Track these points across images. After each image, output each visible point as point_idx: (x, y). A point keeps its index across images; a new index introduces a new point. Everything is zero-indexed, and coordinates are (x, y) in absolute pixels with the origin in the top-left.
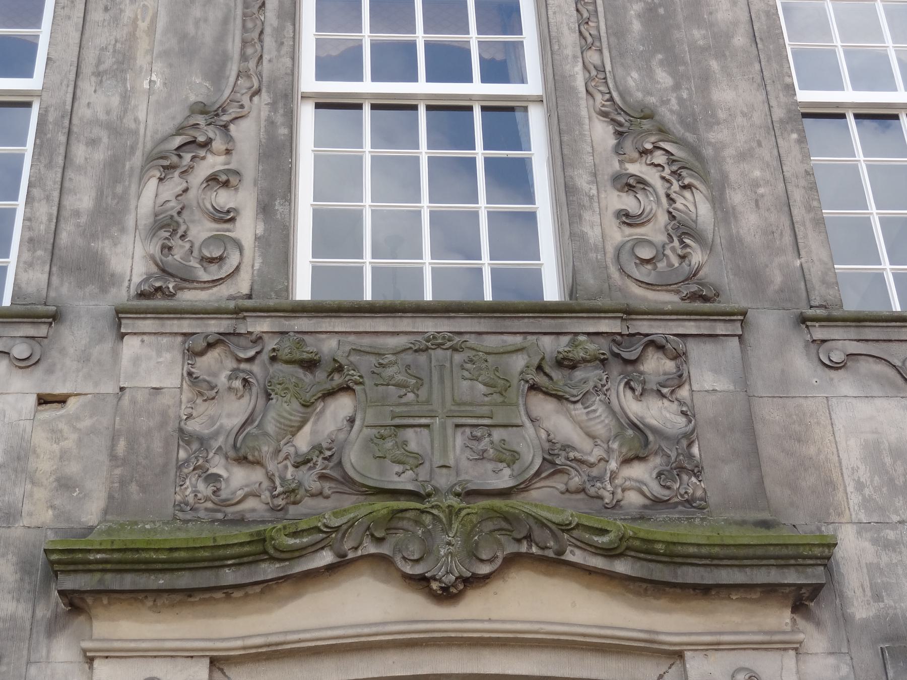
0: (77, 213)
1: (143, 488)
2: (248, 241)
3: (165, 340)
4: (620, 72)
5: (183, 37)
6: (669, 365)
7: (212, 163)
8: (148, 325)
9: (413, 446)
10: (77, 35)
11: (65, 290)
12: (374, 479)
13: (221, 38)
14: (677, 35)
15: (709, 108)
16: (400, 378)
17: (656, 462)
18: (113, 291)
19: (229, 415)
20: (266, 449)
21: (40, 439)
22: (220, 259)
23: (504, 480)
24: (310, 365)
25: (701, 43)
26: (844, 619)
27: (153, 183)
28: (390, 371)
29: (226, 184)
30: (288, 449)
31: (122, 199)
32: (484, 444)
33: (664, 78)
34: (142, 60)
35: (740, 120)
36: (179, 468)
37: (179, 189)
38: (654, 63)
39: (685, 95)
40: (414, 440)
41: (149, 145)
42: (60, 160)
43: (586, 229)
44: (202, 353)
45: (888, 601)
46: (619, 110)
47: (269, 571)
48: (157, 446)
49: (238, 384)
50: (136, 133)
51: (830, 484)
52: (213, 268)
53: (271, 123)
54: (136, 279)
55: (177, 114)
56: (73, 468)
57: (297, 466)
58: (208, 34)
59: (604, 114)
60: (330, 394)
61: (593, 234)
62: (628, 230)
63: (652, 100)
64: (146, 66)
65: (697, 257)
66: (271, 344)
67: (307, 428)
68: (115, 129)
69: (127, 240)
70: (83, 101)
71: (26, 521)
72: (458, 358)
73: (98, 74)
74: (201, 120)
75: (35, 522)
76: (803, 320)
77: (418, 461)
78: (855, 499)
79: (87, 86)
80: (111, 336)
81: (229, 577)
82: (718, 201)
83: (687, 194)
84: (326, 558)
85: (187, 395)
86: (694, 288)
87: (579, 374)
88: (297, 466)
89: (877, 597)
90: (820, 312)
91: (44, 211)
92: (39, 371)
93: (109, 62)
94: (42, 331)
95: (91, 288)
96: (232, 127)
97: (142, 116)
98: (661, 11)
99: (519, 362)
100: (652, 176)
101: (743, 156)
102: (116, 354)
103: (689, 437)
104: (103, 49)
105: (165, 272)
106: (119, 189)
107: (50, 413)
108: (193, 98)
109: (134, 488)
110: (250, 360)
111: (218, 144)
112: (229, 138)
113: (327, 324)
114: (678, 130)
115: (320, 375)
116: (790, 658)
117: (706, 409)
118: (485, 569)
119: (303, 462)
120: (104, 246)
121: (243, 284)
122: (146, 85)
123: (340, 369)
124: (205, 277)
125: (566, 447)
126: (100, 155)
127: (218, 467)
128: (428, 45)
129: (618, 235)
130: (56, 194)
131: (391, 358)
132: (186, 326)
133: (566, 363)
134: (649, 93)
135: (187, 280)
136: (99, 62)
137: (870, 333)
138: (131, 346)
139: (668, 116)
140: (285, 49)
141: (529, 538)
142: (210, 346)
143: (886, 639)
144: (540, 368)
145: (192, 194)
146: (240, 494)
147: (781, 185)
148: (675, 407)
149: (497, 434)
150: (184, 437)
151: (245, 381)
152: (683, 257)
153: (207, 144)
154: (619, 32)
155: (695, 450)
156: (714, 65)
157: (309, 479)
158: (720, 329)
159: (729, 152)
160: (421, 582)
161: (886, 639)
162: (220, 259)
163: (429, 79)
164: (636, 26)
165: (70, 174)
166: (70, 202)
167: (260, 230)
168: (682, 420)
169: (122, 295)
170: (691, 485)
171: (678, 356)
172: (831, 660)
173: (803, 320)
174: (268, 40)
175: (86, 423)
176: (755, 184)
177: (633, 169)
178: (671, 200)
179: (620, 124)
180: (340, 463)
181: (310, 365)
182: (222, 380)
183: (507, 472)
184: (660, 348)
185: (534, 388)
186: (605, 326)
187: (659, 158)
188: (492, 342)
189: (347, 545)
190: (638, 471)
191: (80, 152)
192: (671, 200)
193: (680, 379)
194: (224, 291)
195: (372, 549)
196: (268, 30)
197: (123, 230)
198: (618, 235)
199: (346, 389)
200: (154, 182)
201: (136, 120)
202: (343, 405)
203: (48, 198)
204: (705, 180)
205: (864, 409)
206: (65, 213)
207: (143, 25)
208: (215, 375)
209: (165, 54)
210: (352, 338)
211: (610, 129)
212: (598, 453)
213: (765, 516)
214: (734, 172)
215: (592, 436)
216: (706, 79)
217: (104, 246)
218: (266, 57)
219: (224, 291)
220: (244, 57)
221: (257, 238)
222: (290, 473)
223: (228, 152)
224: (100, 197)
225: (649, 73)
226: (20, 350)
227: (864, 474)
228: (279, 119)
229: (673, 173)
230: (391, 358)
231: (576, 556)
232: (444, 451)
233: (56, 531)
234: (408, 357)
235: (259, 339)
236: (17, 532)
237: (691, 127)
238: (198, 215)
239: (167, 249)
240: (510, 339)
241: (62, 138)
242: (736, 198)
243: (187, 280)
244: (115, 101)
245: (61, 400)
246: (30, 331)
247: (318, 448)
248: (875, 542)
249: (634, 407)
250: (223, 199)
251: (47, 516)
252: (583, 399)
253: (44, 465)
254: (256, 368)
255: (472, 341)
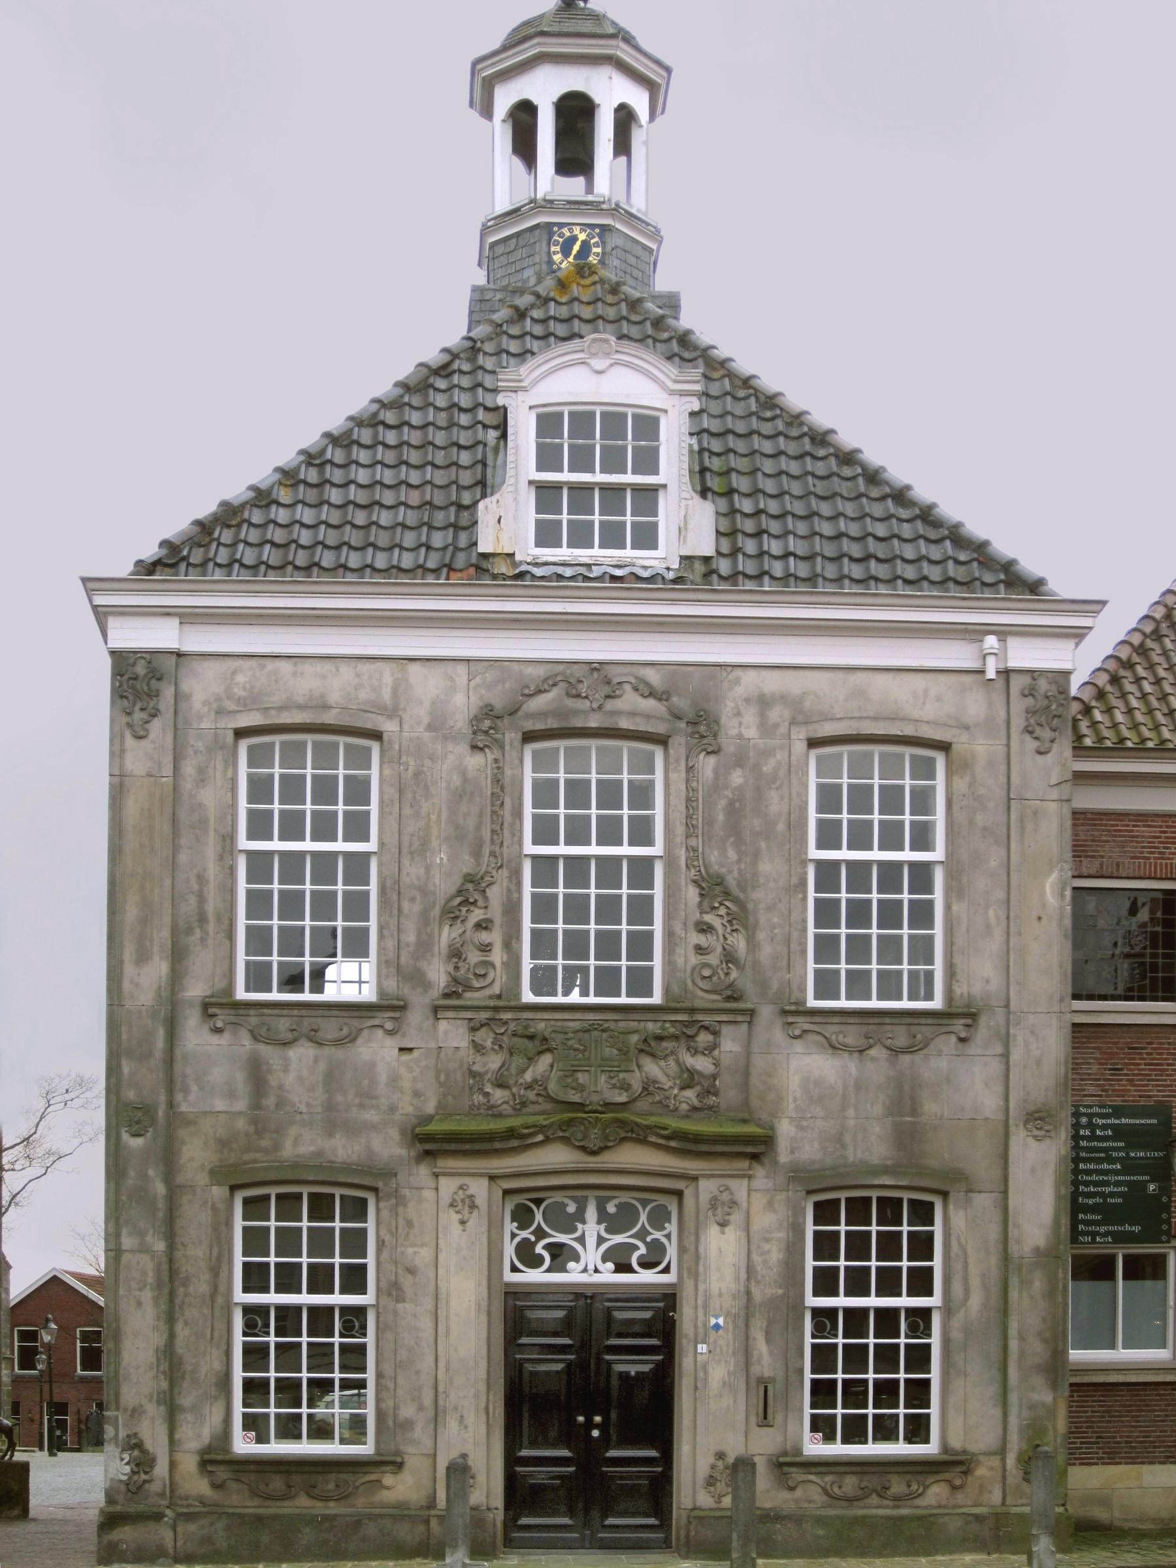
0: (408, 945)
1: (454, 1097)
2: (498, 964)
3: (459, 1022)
4: (707, 850)
5: (457, 826)
6: (710, 1038)
7: (477, 915)
8: (451, 1014)
9: (581, 1081)
10: (396, 826)
11: (406, 991)
12: (562, 1096)
13: (478, 827)
14: (744, 823)
15: (755, 875)
16: (576, 1046)
17: (698, 1088)
18: (431, 991)
19: (493, 1062)
20: (511, 1082)
21: (403, 1071)
22: (484, 976)
23: (622, 1098)
24: (531, 1037)
25: (758, 829)
26: (775, 1163)
27: (446, 929)
28: (570, 1043)
29: (486, 928)
30: (521, 1081)
31: (431, 936)
32: (614, 1081)
33: (732, 855)
34: (435, 843)
35: (772, 884)
36: (471, 1089)
37: (461, 931)
38: (728, 844)
39: (743, 866)
40: (582, 1078)
41: (443, 902)
42: (396, 912)
43: (676, 958)
44: (478, 1029)
45: (797, 1155)
46: (703, 879)
47: (515, 1143)
48: (459, 1076)
49: (496, 1047)
50: (434, 893)
51: (781, 1098)
52: (481, 980)
53: (509, 890)
54: (442, 985)
55: (456, 882)
56: (420, 1086)
57: (526, 1089)
58: (471, 824)
59: (695, 882)
60: (540, 1053)
61: (680, 961)
62: (700, 957)
63: (723, 870)
64: (437, 848)
65: (734, 974)
66: (512, 1026)
67: (530, 1069)
68: (423, 891)
69: (436, 961)
70: (404, 872)
71: (401, 1111)
72: (605, 1035)
73: (411, 853)
74: (470, 886)
75: (405, 1112)
76: (785, 1013)
77: (580, 1088)
78: (792, 1106)
79: (406, 862)
80: (431, 1021)
81: (497, 1145)
82: (751, 940)
83: (735, 934)
84: (540, 1138)
85: (471, 1051)
86: (729, 993)
87: (665, 1044)
88: (526, 1089)
89: (792, 1152)
90: (793, 1008)
91: (391, 944)
92: (398, 1036)
93: (416, 845)
94: (397, 1015)
95: (419, 990)
96: (487, 890)
97: (437, 882)
98: (737, 805)
99: (634, 1038)
100: (717, 923)
101: (770, 909)
102: (435, 1027)
103: (714, 1077)
104: (412, 835)
105: (456, 981)
106: (429, 930)
107: (406, 1057)
108: (465, 870)
109: (450, 1098)
110: (502, 1034)
111: (480, 903)
112: (486, 898)
113: (539, 1015)
114: (735, 891)
115: (537, 1042)
116: (745, 1182)
117: (726, 1061)
118: (611, 1144)
119: (529, 1087)
120: (423, 964)
121: (496, 989)
122: (438, 861)
123: (545, 1039)
124: (477, 985)
125: (655, 1082)
126: (417, 908)
127: (488, 1088)
128: (599, 782)
129: (694, 960)
130: (396, 934)
131: (571, 1035)
132: (469, 1015)
133: (660, 1038)
134: (722, 866)
135: (468, 987)
136: (411, 845)
137: (817, 1019)
138: (443, 1025)
139: (731, 882)
140: (516, 839)
141: (632, 1131)
142: (482, 1026)
143: (794, 1171)
144: (645, 1040)
145: (468, 933)
146: (499, 1102)
147: (787, 928)
148: (710, 1060)
149: (622, 1075)
150: (473, 1074)
151: (500, 1046)
152: (727, 974)
153: (475, 903)
154: (709, 822)
155: (717, 1083)
156: (763, 845)
157: (531, 1095)
158: (739, 1018)
159: (762, 906)
160: (583, 1149)
161: (794, 1171)
162: (484, 976)
163: (601, 472)
164: (721, 817)
165: (402, 920)
166: (403, 937)
167: (505, 959)
168: (713, 1067)
169: (435, 993)
170: (712, 1100)
171: (716, 1033)
172: (765, 1181)
173: (785, 1013)
174: (506, 833)
175: (423, 1063)
176: (773, 927)
177: (708, 918)
178: (725, 939)
179: (703, 888)
180: (546, 1089)
181: (531, 1037)
182: (489, 1043)
183: (625, 1094)
184: (706, 1028)
185: (642, 1051)
186: (680, 1017)
187: (722, 911)
188: (622, 1024)
189: (549, 1133)
190: (690, 1094)
191: (406, 905)
192: (725, 939)
193: (714, 1046)
194: (487, 992)
195: (561, 1134)
196: (506, 825)
197: (432, 955)
198: (694, 960)
199: (549, 1050)
200: (447, 927)
201: (434, 884)
202: (547, 1059)
203: (392, 936)
204: (745, 927)
205: (807, 1060)
206: (402, 945)
207: (434, 817)
208: (485, 1041)
209: (447, 839)
210: (552, 1023)
211: (697, 890)
212: (670, 1084)
213: (746, 1116)
214: (762, 919)
215: (668, 1076)
216: (757, 855)
217: (423, 964)
218: (505, 844)
219: (487, 992)
220: (492, 842)
221: (503, 963)
222: (522, 1092)
223: (486, 907)
224: (419, 935)
225: (723, 852)
226: (389, 1026)
227: (798, 1094)
228: (513, 888)
229: (729, 921)
230: (571, 1035)
231: (653, 1139)
232: (596, 1085)
233: (415, 1116)
234: (580, 1035)
235: (505, 1023)
236: (397, 1117)
237: (743, 889)
238: (471, 946)
239: (457, 968)
240: (632, 1024)
241: (395, 897)
242: (761, 936)
243: (468, 987)
244: (422, 871)
245: (410, 1050)
246: (392, 1014)
247: (535, 1081)
248: (797, 1127)
249: (690, 1061)
250: (484, 937)
251: (410, 1109)
252: (665, 1057)
253: (406, 1084)
254: (505, 1038)
255: (612, 1026)
